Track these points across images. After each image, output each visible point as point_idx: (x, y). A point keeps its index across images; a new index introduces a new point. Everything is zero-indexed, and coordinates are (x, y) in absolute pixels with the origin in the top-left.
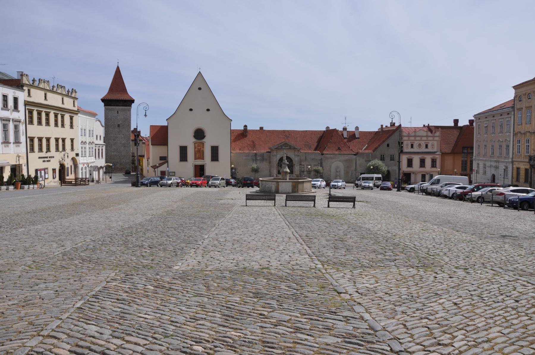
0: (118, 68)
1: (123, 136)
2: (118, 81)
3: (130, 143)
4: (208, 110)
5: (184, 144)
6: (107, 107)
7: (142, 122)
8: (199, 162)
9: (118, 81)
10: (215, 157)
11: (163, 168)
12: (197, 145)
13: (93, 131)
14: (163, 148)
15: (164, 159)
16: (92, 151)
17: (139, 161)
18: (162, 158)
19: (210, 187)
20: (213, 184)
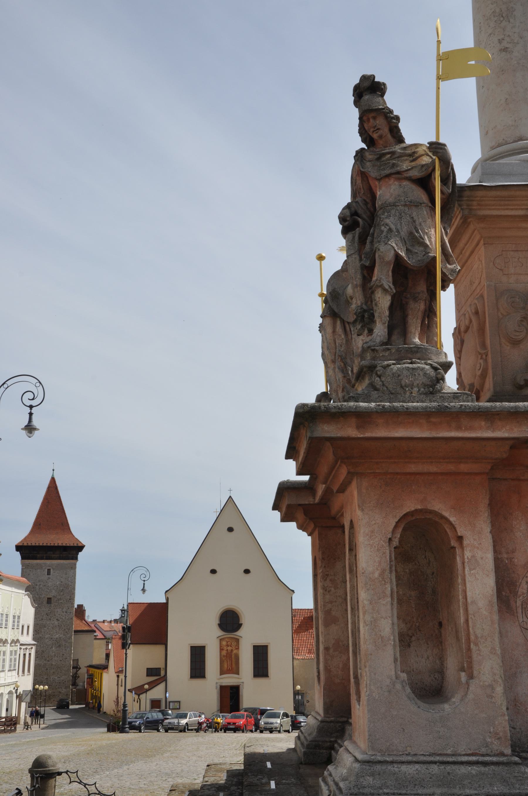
0: (53, 480)
1: (56, 623)
2: (52, 512)
3: (70, 638)
4: (247, 571)
5: (198, 642)
6: (27, 562)
7: (101, 595)
8: (230, 680)
9: (52, 512)
10: (261, 669)
11: (157, 693)
12: (224, 643)
13: (19, 617)
14: (157, 650)
15: (157, 675)
16: (15, 659)
17: (91, 677)
18: (151, 672)
19: (261, 732)
20: (268, 726)
